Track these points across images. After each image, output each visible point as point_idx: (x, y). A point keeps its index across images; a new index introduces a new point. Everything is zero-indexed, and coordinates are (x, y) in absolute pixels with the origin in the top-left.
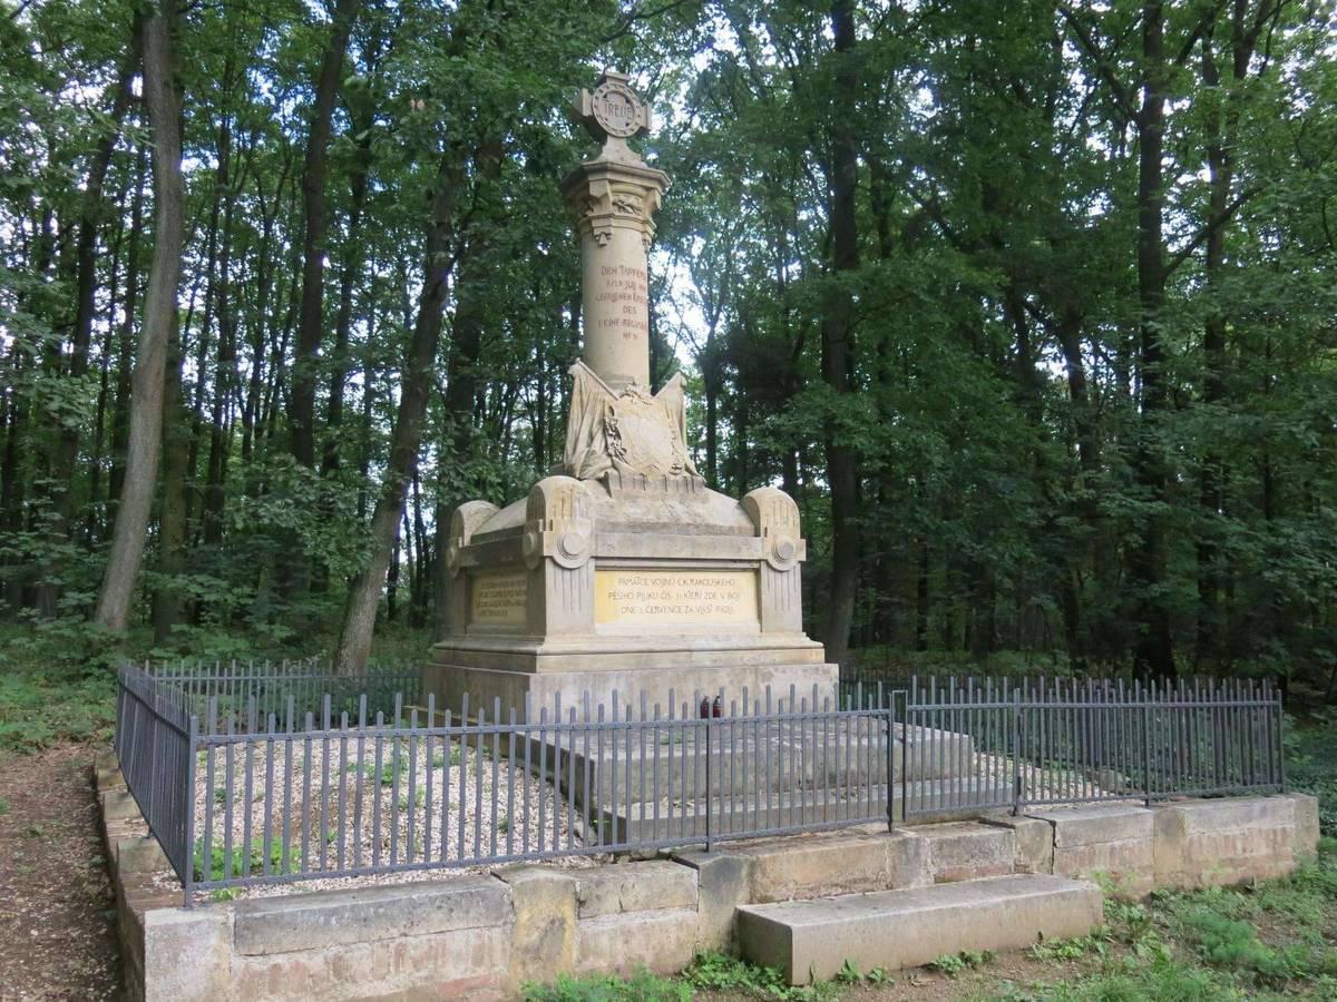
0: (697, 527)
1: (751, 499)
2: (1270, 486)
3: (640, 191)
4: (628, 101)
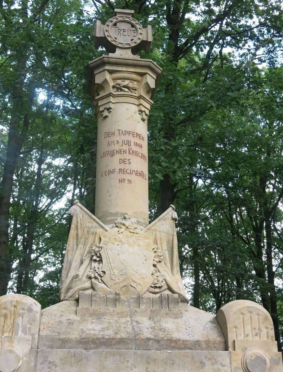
0: (158, 341)
1: (221, 310)
2: (128, 367)
3: (134, 76)
4: (133, 26)
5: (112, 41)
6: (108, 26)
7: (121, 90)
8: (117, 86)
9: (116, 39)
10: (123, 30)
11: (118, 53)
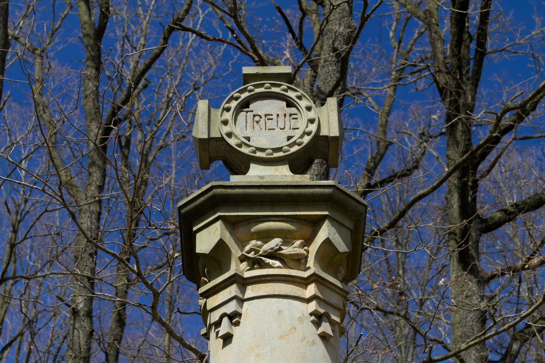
4: (290, 104)
5: (272, 154)
6: (106, 60)
7: (262, 265)
8: (249, 255)
9: (248, 139)
10: (266, 115)
11: (257, 174)
